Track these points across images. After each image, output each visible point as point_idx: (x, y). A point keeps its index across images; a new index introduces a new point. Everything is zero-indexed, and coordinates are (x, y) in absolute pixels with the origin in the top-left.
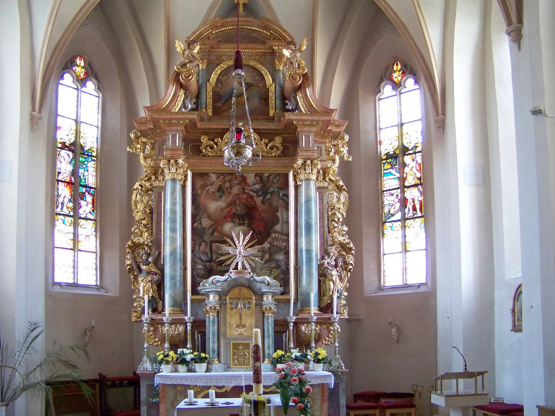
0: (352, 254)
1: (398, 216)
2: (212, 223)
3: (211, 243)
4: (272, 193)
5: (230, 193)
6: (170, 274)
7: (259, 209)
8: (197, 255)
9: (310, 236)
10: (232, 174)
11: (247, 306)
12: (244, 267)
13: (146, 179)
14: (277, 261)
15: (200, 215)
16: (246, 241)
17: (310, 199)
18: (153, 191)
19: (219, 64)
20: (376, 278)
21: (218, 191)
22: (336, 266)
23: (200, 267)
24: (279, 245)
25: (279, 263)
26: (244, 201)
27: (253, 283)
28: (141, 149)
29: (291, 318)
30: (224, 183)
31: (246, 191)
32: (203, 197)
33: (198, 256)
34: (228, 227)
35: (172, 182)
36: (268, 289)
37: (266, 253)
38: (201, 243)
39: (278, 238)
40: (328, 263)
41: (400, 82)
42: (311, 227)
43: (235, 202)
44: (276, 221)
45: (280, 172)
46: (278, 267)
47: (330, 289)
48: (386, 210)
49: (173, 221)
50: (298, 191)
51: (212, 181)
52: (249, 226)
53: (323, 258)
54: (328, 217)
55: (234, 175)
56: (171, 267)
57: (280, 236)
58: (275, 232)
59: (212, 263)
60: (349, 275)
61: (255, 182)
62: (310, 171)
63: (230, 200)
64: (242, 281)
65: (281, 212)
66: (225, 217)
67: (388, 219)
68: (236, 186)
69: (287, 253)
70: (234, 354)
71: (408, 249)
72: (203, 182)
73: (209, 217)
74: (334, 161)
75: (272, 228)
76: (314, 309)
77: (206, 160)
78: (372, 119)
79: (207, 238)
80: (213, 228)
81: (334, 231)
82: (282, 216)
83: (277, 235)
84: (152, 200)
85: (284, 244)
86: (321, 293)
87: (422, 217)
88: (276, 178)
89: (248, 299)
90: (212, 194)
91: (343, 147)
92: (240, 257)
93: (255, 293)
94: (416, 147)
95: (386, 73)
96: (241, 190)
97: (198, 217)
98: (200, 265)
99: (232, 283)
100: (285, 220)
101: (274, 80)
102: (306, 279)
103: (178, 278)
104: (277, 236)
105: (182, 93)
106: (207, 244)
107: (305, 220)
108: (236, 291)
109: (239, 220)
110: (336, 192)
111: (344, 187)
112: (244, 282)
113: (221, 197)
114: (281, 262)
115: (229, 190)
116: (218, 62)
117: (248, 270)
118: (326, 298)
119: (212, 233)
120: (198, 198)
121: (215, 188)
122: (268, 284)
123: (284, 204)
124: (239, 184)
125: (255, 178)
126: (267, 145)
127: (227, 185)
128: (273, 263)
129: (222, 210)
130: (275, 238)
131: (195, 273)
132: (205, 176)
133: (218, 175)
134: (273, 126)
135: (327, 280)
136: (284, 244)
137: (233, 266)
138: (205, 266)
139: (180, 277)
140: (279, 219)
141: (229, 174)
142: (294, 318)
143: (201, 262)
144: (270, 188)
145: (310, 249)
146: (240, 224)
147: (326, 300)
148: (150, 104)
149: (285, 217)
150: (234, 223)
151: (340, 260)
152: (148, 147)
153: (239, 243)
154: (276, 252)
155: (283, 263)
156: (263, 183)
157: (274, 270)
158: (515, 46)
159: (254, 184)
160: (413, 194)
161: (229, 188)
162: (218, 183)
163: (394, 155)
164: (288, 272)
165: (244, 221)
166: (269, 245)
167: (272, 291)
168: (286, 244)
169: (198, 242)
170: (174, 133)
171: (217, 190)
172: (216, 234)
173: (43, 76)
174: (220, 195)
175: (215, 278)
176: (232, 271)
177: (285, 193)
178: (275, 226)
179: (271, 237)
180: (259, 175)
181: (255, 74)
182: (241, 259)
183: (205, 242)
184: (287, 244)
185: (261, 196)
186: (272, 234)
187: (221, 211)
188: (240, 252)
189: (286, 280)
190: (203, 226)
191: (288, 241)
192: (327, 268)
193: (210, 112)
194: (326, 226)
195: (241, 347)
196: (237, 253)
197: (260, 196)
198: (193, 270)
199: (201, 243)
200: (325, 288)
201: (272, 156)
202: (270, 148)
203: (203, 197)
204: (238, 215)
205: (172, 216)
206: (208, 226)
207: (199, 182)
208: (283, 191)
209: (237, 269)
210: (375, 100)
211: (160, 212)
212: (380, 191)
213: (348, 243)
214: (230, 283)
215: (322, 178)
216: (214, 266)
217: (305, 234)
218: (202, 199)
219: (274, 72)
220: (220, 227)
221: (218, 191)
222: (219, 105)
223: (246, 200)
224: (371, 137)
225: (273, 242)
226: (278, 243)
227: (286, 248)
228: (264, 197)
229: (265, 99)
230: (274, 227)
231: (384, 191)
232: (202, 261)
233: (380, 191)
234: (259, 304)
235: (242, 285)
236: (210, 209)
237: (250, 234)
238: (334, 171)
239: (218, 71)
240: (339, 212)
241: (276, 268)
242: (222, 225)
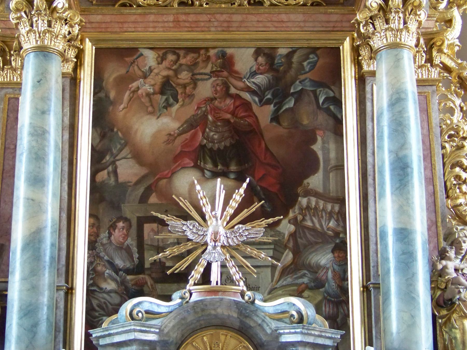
2: (143, 171)
4: (299, 95)
5: (191, 96)
6: (21, 300)
7: (268, 135)
8: (102, 254)
9: (408, 192)
15: (115, 151)
16: (234, 204)
17: (403, 96)
23: (110, 286)
24: (318, 226)
25: (321, 274)
26: (228, 116)
27: (255, 318)
30: (176, 72)
31: (233, 91)
32: (122, 106)
33: (106, 258)
35: (36, 56)
36: (302, 333)
37: (286, 247)
38: (115, 223)
39: (316, 208)
40: (456, 270)
42: (409, 170)
43: (205, 116)
45: (314, 44)
49: (91, 34)
50: (364, 88)
51: (147, 68)
53: (443, 255)
54: (443, 156)
55: (202, 52)
56: (24, 279)
57: (321, 203)
58: (308, 193)
59: (141, 276)
61: (254, 69)
62: (401, 26)
63: (193, 113)
64: (222, 311)
65: (324, 143)
66: (178, 157)
68: (207, 80)
72: (123, 71)
75: (300, 183)
81: (461, 191)
82: (326, 151)
83: (313, 200)
85: (332, 224)
88: (308, 58)
90: (145, 100)
92: (215, 247)
96: (218, 88)
97: (108, 158)
98: (109, 281)
100: (333, 163)
102: (400, 311)
103: (44, 313)
104: (313, 204)
106: (130, 226)
107: (390, 152)
108: (204, 343)
110: (458, 95)
112: (226, 313)
113: (168, 106)
114: (327, 272)
117: (239, 285)
119: (144, 199)
120: (111, 108)
121: (153, 85)
122: (301, 320)
123: (331, 122)
124: (214, 73)
125: (256, 60)
127: (185, 76)
128: (304, 275)
129: (171, 138)
130: (308, 207)
131: (95, 303)
132: (131, 55)
133: (161, 53)
135: (455, 315)
136: (332, 224)
137: (196, 274)
138: (123, 283)
139: (48, 308)
141: (189, 50)
143: (113, 274)
144: (293, 83)
145: (408, 227)
149: (333, 155)
150: (202, 170)
153: (213, 209)
154: (311, 245)
155: (330, 274)
156: (277, 71)
159: (253, 74)
161: (189, 84)
164: (343, 298)
165: (227, 165)
166: (292, 228)
167: (310, 339)
168: (338, 225)
169: (106, 221)
171: (157, 88)
174: (167, 100)
175: (139, 303)
176: (192, 288)
177: (332, 94)
178: (307, 176)
179: (297, 207)
182: (220, 254)
183: (126, 220)
184: (341, 224)
185: (271, 104)
186: (300, 199)
187: (168, 142)
188: (216, 234)
189: (339, 320)
190: (121, 180)
192: (456, 282)
194: (440, 178)
196: (208, 239)
197: (268, 102)
198: (90, 293)
199: (115, 223)
200: (451, 340)
203: (122, 106)
204: (211, 150)
205: (34, 143)
206: (134, 180)
208: (327, 90)
209: (209, 282)
211: (12, 147)
214: (184, 319)
215: (424, 59)
216: (146, 283)
217: (392, 186)
220: (164, 181)
221: (162, 92)
223: (233, 114)
225: (304, 219)
226: (315, 220)
227: (337, 234)
228: (279, 105)
230: (306, 182)
232: (116, 270)
236: (139, 134)
241: (311, 289)
242: (170, 177)
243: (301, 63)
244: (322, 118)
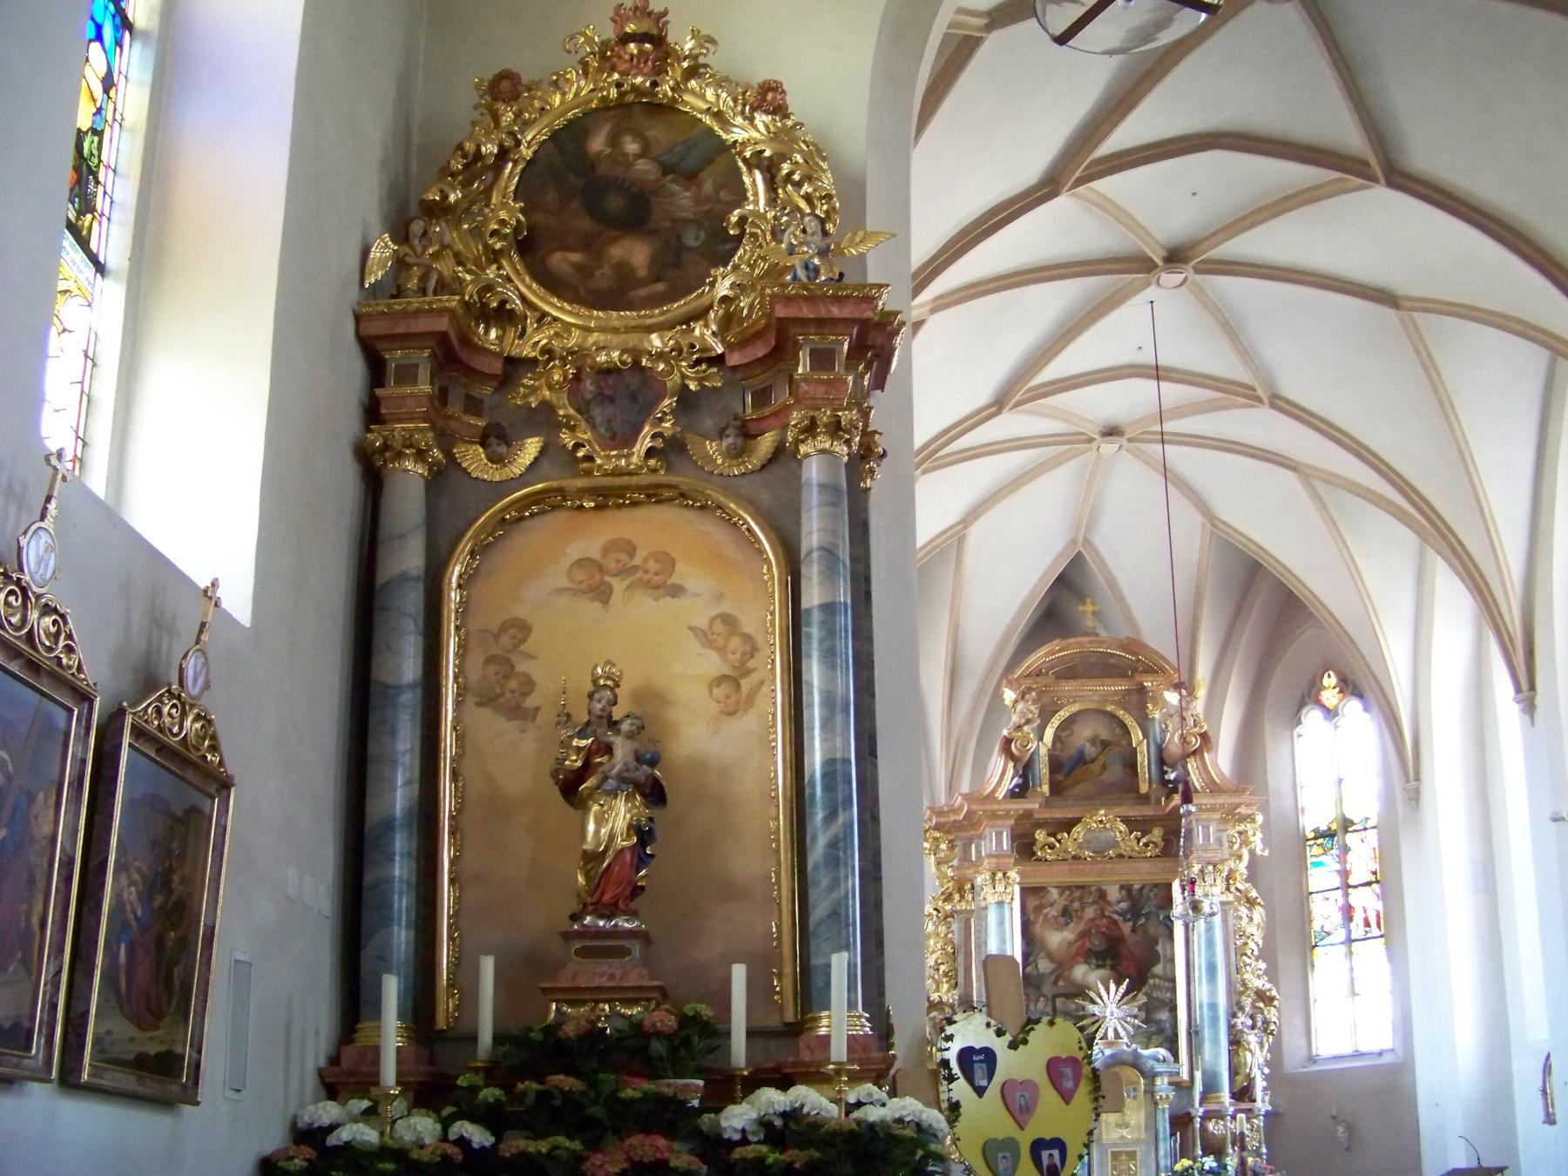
0: (1275, 1007)
1: (1340, 935)
2: (1054, 966)
3: (1055, 997)
4: (1148, 916)
5: (1081, 918)
10: (1083, 887)
11: (1132, 1094)
12: (1117, 1036)
13: (943, 897)
14: (1158, 1022)
18: (953, 917)
19: (1057, 712)
20: (1303, 1042)
21: (1063, 915)
22: (1253, 1027)
26: (1104, 930)
28: (930, 850)
29: (1197, 1111)
30: (1072, 902)
31: (1107, 913)
34: (1080, 972)
41: (1336, 708)
43: (1090, 930)
44: (1154, 958)
46: (1160, 1031)
47: (1245, 1064)
48: (1316, 926)
52: (1113, 968)
53: (1234, 1015)
57: (1162, 983)
58: (1155, 976)
60: (1271, 1040)
65: (1163, 945)
67: (1321, 940)
69: (1173, 1009)
70: (1114, 1168)
71: (1357, 992)
73: (1050, 957)
74: (1240, 857)
75: (1149, 971)
76: (1225, 1096)
77: (1043, 867)
78: (1289, 771)
79: (1048, 989)
80: (1056, 974)
83: (1157, 980)
84: (952, 932)
86: (1234, 1071)
87: (1382, 936)
89: (1133, 1083)
90: (1054, 922)
91: (1254, 835)
93: (1143, 1074)
94: (1367, 819)
95: (1310, 691)
99: (1110, 1061)
100: (1168, 957)
101: (1145, 736)
105: (1011, 764)
107: (1206, 959)
109: (1097, 960)
111: (1259, 900)
113: (1067, 924)
115: (1079, 913)
116: (1054, 709)
118: (1239, 1078)
119: (1055, 983)
123: (1167, 931)
124: (1094, 903)
126: (1139, 840)
127: (1076, 905)
129: (1070, 944)
134: (1147, 811)
140: (1159, 955)
142: (1201, 1110)
146: (1099, 967)
147: (1241, 1081)
148: (971, 788)
149: (1169, 952)
150: (1089, 964)
151: (1259, 1018)
152: (943, 846)
154: (1157, 1008)
155: (1168, 1025)
157: (1154, 1037)
158: (1527, 718)
159: (1119, 902)
160: (1366, 901)
162: (1062, 903)
163: (1329, 832)
165: (1104, 960)
169: (1033, 997)
170: (999, 829)
171: (1060, 913)
172: (1061, 983)
173: (361, 557)
178: (1153, 966)
180: (1126, 888)
181: (1114, 726)
183: (1045, 996)
188: (1112, 1012)
190: (1041, 971)
191: (1174, 990)
192: (1242, 1031)
193: (1046, 788)
195: (1124, 1157)
197: (1129, 920)
201: (1146, 857)
202: (1144, 844)
207: (1032, 902)
210: (1292, 737)
212: (1305, 893)
213: (1269, 990)
218: (1037, 928)
219: (1144, 722)
221: (1063, 915)
222: (1059, 777)
223: (1108, 928)
224: (1288, 803)
228: (1135, 924)
229: (1131, 764)
231: (1311, 893)
233: (1305, 893)
234: (1150, 1092)
235: (1124, 1063)
237: (1126, 983)
238: (1241, 874)
239: (1055, 722)
240: (1253, 940)
243: (1148, 894)
244: (1162, 930)
